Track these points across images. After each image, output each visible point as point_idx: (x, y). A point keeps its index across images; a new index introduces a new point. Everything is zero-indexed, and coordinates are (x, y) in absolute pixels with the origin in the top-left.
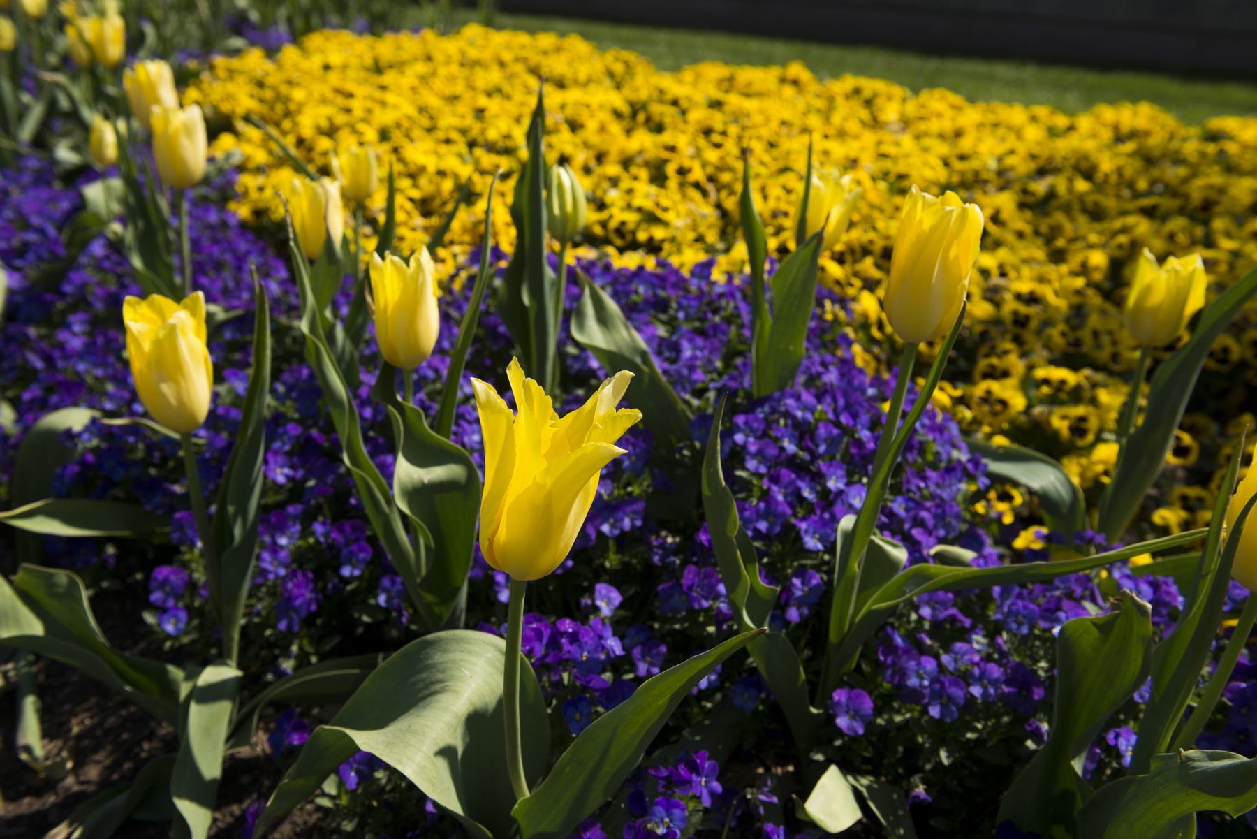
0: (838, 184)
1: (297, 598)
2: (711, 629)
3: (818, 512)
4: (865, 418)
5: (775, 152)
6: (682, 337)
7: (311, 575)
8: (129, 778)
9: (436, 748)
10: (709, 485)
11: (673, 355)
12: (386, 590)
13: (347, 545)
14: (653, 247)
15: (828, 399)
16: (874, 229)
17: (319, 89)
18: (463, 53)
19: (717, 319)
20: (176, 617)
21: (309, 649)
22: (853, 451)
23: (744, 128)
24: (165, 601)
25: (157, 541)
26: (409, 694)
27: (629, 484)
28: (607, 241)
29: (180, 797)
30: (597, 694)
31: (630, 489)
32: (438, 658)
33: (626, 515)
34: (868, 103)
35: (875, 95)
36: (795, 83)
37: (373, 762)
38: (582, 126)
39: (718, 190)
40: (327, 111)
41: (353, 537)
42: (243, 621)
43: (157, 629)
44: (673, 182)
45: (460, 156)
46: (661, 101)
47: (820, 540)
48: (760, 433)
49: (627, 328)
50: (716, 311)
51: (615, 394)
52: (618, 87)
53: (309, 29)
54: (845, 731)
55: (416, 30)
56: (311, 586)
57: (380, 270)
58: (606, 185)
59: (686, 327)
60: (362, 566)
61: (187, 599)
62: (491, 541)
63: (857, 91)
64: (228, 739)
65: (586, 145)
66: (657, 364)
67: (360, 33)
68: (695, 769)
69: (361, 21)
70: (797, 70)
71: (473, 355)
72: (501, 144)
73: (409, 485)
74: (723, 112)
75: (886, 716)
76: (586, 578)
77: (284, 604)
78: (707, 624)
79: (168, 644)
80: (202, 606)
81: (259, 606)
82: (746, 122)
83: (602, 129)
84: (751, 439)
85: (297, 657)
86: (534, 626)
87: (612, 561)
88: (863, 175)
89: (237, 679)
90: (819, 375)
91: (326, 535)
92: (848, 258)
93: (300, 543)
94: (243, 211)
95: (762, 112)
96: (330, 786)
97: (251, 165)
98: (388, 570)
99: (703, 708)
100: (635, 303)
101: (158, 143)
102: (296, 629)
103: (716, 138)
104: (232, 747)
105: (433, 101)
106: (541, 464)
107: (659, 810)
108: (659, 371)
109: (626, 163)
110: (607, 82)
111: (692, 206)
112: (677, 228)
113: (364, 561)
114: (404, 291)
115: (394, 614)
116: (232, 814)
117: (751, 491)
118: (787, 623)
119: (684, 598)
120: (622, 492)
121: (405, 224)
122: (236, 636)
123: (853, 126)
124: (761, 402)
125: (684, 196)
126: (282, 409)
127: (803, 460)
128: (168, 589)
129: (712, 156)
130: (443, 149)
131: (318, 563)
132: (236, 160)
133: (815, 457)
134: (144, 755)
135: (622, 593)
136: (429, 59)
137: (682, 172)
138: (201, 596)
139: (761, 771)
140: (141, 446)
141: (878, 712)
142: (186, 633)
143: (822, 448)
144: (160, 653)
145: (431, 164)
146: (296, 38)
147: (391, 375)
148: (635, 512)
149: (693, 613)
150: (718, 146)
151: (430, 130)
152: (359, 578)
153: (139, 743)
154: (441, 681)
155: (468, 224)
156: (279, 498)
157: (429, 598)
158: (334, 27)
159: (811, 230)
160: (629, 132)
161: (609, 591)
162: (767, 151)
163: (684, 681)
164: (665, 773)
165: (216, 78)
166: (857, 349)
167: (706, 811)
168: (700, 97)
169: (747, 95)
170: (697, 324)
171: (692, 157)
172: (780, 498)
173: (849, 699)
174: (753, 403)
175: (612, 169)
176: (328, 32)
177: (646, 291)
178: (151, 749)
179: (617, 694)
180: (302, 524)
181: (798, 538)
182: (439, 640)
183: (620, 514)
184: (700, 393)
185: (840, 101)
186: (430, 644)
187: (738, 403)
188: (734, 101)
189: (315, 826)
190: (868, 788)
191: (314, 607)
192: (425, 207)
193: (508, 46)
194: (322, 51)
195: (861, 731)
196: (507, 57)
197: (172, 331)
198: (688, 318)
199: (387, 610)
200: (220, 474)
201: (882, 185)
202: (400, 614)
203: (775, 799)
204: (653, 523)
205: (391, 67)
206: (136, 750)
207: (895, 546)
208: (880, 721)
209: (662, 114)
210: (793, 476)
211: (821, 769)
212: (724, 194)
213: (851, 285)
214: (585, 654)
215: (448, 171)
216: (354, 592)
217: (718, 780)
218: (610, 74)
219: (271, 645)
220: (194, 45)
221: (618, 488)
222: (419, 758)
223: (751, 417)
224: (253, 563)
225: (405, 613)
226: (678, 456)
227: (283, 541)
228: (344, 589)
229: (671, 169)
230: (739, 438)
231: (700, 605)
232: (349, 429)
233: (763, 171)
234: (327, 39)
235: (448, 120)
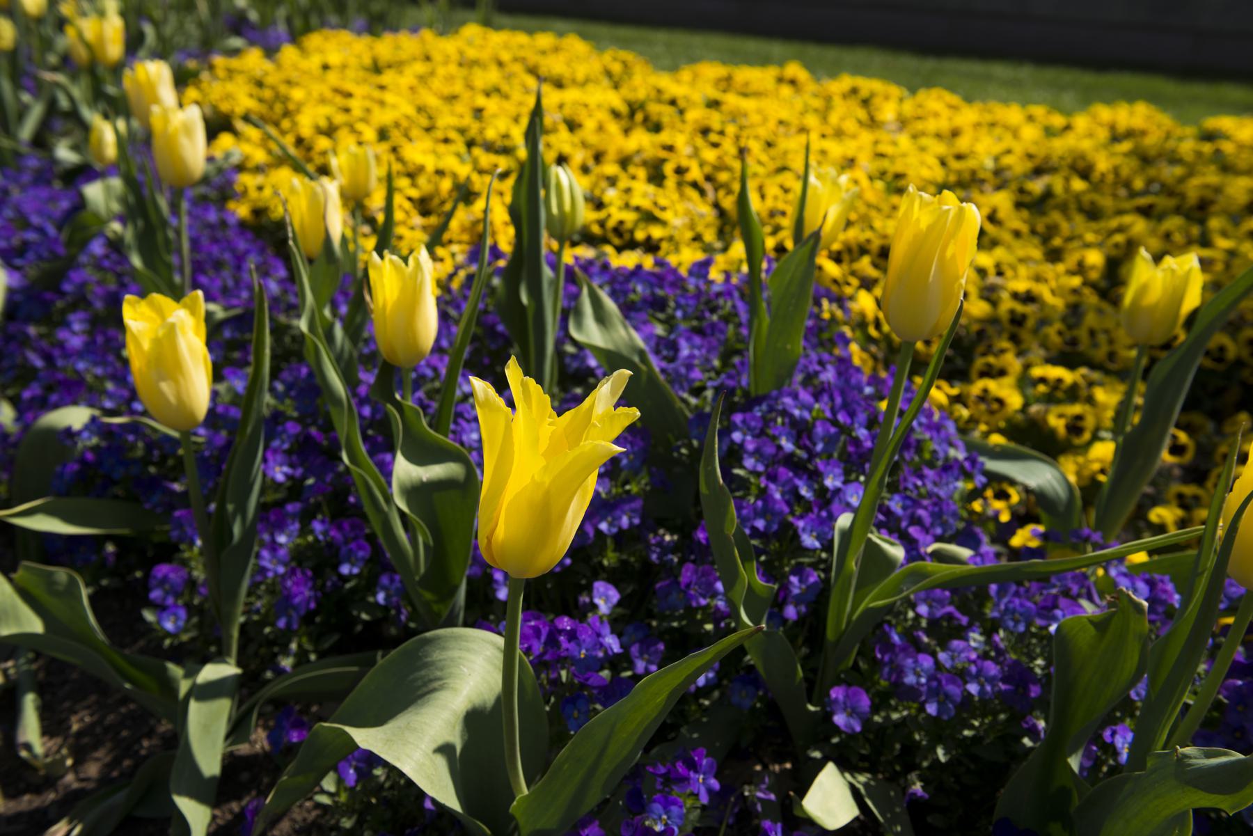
0: (835, 183)
1: (296, 595)
2: (709, 627)
3: (816, 510)
4: (862, 416)
5: (773, 152)
6: (680, 335)
7: (310, 573)
9: (435, 746)
10: (707, 484)
11: (671, 353)
12: (384, 588)
13: (346, 543)
14: (651, 246)
15: (826, 398)
16: (872, 228)
17: (318, 89)
18: (461, 53)
19: (715, 318)
20: (175, 614)
21: (308, 646)
22: (850, 449)
23: (741, 128)
24: (164, 599)
25: (156, 539)
26: (408, 692)
27: (627, 482)
28: (605, 240)
29: (180, 794)
30: (595, 692)
31: (628, 487)
32: (436, 655)
33: (624, 513)
34: (866, 103)
35: (872, 95)
36: (793, 82)
37: (371, 759)
38: (580, 126)
39: (716, 190)
40: (326, 110)
41: (352, 535)
42: (242, 619)
43: (157, 627)
44: (671, 182)
45: (458, 155)
46: (659, 101)
47: (818, 538)
48: (757, 431)
49: (625, 327)
50: (713, 310)
51: (613, 392)
52: (616, 86)
53: (308, 29)
54: (843, 728)
55: (414, 30)
56: (310, 584)
57: (379, 269)
58: (604, 184)
59: (684, 326)
60: (361, 564)
61: (186, 597)
62: (489, 539)
63: (854, 91)
64: (227, 737)
65: (584, 145)
66: (655, 363)
67: (359, 33)
68: (693, 766)
69: (360, 21)
70: (794, 69)
71: (472, 354)
72: (499, 143)
73: (408, 484)
74: (721, 112)
75: (883, 714)
76: (584, 576)
77: (283, 602)
78: (704, 621)
79: (167, 642)
80: (201, 604)
81: (259, 604)
82: (743, 121)
83: (601, 128)
84: (749, 438)
85: (296, 655)
86: (533, 623)
87: (610, 559)
89: (236, 676)
90: (817, 374)
91: (325, 533)
92: (846, 257)
93: (299, 541)
94: (242, 211)
95: (759, 111)
96: (329, 783)
97: (250, 165)
98: (387, 568)
99: (701, 705)
100: (633, 302)
101: (158, 143)
102: (295, 626)
103: (713, 137)
104: (231, 744)
105: (432, 101)
106: (539, 462)
107: (657, 807)
108: (657, 370)
109: (624, 162)
110: (605, 82)
111: (690, 206)
112: (675, 228)
113: (363, 559)
114: (403, 290)
115: (393, 612)
116: (231, 811)
117: (748, 489)
118: (784, 621)
119: (681, 595)
120: (620, 490)
121: (404, 223)
122: (235, 633)
123: (850, 126)
124: (758, 400)
125: (682, 195)
126: (281, 408)
127: (800, 458)
128: (167, 587)
129: (710, 155)
130: (442, 148)
131: (317, 561)
132: (235, 159)
133: (812, 455)
134: (143, 752)
135: (620, 591)
136: (428, 58)
137: (680, 171)
138: (200, 594)
139: (758, 768)
140: (140, 444)
141: (875, 709)
142: (186, 630)
143: (819, 447)
144: (159, 650)
145: (430, 163)
146: (295, 37)
147: (390, 374)
148: (633, 511)
149: (690, 611)
150: (715, 145)
151: (428, 130)
152: (358, 576)
153: (138, 741)
154: (440, 679)
155: (467, 224)
156: (278, 496)
157: (428, 596)
158: (333, 27)
159: (809, 229)
160: (627, 132)
161: (607, 589)
162: (764, 150)
163: (682, 679)
164: (663, 770)
166: (854, 347)
167: (704, 808)
168: (697, 97)
169: (745, 95)
170: (695, 323)
171: (690, 157)
172: (778, 496)
173: (847, 696)
175: (610, 169)
176: (327, 32)
177: (644, 290)
178: (150, 747)
179: (615, 691)
180: (301, 522)
181: (796, 537)
182: (438, 638)
183: (618, 512)
184: (698, 392)
185: (837, 101)
186: (428, 642)
187: (736, 402)
188: (732, 100)
189: (314, 823)
190: (866, 785)
191: (313, 605)
192: (424, 206)
193: (506, 46)
194: (321, 51)
195: (858, 728)
196: (506, 56)
197: (171, 330)
198: (686, 317)
199: (386, 608)
200: (219, 472)
201: (880, 185)
202: (399, 612)
203: (772, 797)
204: (651, 521)
205: (389, 66)
206: (136, 747)
207: (892, 544)
208: (877, 718)
209: (660, 114)
210: (791, 474)
211: (819, 766)
212: (721, 193)
213: (848, 284)
214: (583, 651)
215: (447, 171)
216: (352, 590)
217: (716, 777)
218: (608, 74)
219: (270, 642)
220: (194, 45)
221: (616, 486)
222: (418, 755)
223: (748, 415)
224: (252, 561)
225: (404, 611)
226: (675, 454)
227: (282, 539)
228: (343, 587)
229: (668, 169)
230: (737, 436)
231: (698, 603)
232: (348, 428)
234: (326, 39)
235: (447, 120)
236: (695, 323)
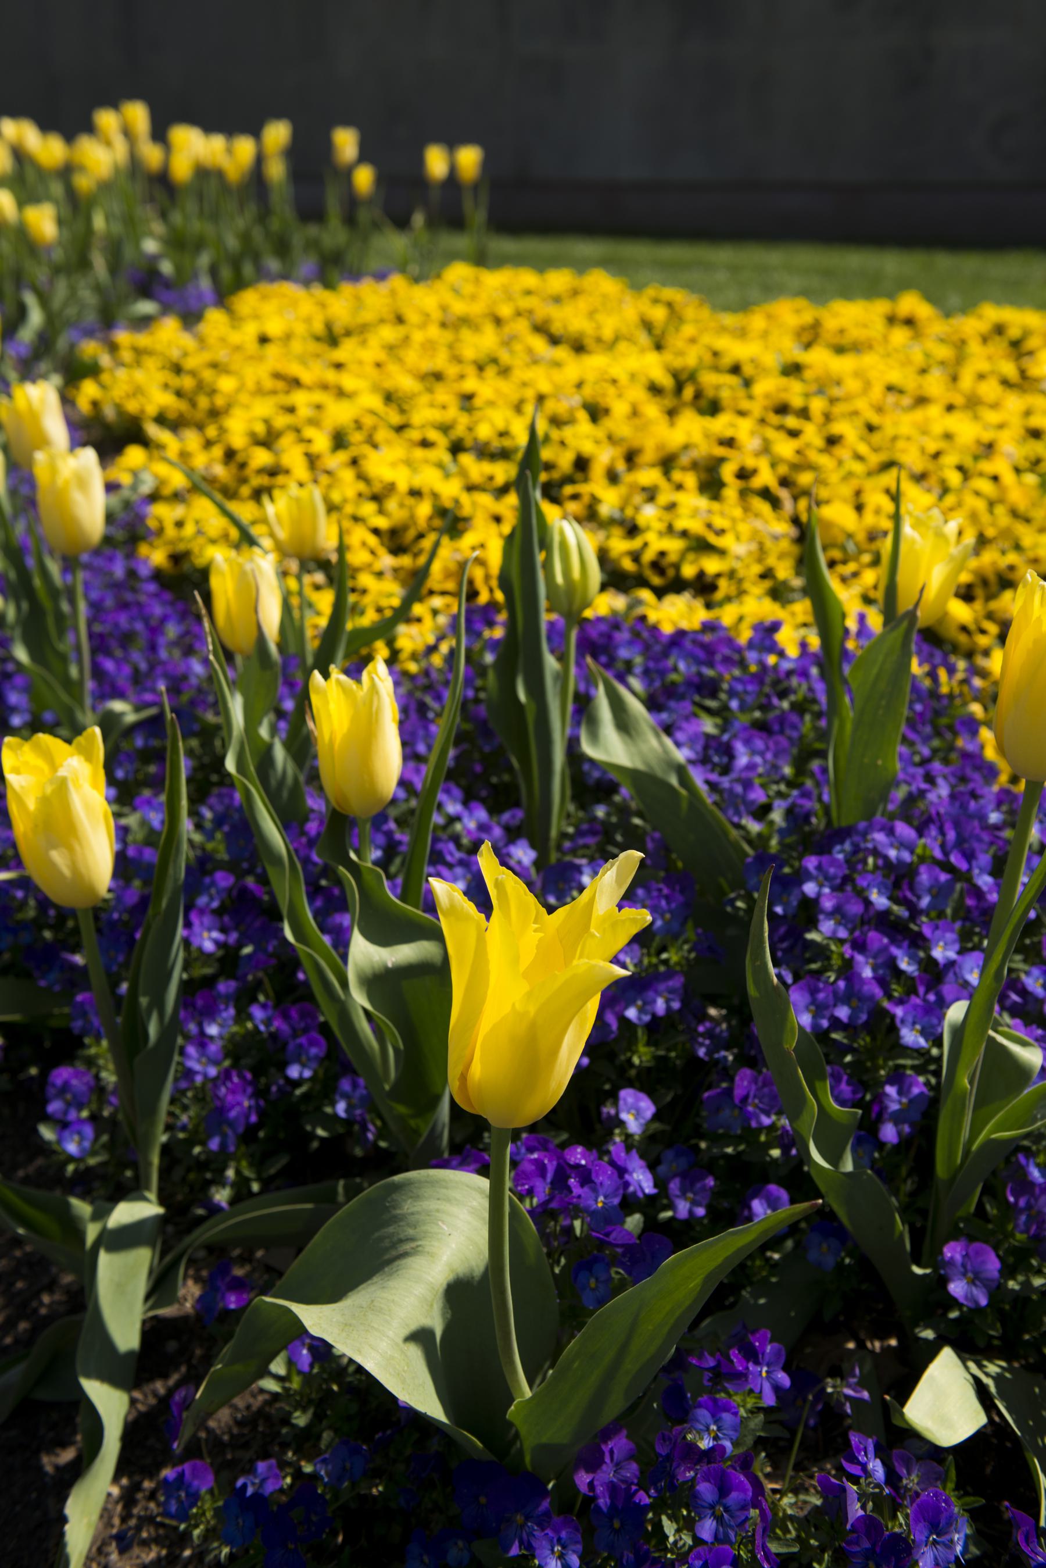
0: (939, 535)
1: (232, 1107)
2: (776, 1153)
3: (921, 990)
4: (984, 858)
5: (876, 438)
6: (735, 736)
7: (249, 1076)
8: (26, 1342)
9: (406, 1332)
10: (756, 983)
11: (725, 760)
12: (346, 1096)
13: (295, 1036)
14: (704, 587)
15: (933, 832)
16: (1018, 547)
17: (257, 373)
18: (444, 308)
19: (785, 705)
20: (79, 1133)
21: (247, 1173)
22: (970, 902)
23: (833, 401)
24: (66, 1113)
25: (54, 1023)
26: (373, 1254)
27: (664, 949)
28: (642, 582)
29: (89, 1376)
30: (619, 1250)
31: (664, 956)
32: (408, 1207)
33: (660, 995)
34: (1018, 348)
35: (1027, 333)
36: (909, 322)
37: (322, 1350)
38: (607, 411)
39: (795, 498)
40: (264, 408)
41: (302, 1025)
42: (164, 1138)
43: (55, 1147)
44: (731, 493)
45: (440, 466)
46: (716, 369)
47: (923, 1033)
49: (658, 736)
50: (783, 695)
51: (619, 881)
52: (659, 347)
53: (240, 284)
54: (962, 1300)
55: (381, 276)
56: (250, 1090)
57: (323, 693)
58: (638, 499)
59: (744, 719)
60: (314, 1065)
61: (94, 1106)
62: (463, 1078)
63: (999, 329)
64: (147, 1298)
65: (611, 438)
66: (698, 777)
67: (306, 283)
68: (752, 1355)
69: (307, 264)
70: (911, 303)
71: (457, 759)
72: (496, 444)
73: (369, 971)
74: (803, 380)
75: (1021, 1278)
76: (608, 1080)
77: (216, 1117)
78: (769, 1145)
79: (71, 1168)
80: (113, 1115)
81: (184, 1118)
82: (835, 392)
83: (635, 413)
84: (826, 890)
85: (233, 1185)
86: (535, 1156)
87: (641, 1056)
88: (1000, 466)
89: (157, 1218)
90: (922, 793)
91: (268, 1022)
92: (979, 592)
93: (235, 1029)
94: (157, 557)
95: (858, 374)
96: (278, 1366)
97: (167, 491)
98: (347, 1068)
99: (768, 1260)
100: (673, 684)
101: (43, 498)
102: (232, 1149)
103: (791, 422)
104: (151, 1308)
105: (406, 383)
106: (528, 973)
107: (703, 1414)
108: (702, 788)
109: (667, 463)
110: (643, 339)
111: (758, 524)
112: (738, 558)
113: (316, 1057)
114: (355, 720)
115: (356, 1127)
116: (155, 1394)
117: (829, 958)
118: (880, 1145)
119: (736, 1112)
120: (654, 960)
121: (368, 567)
122: (155, 1160)
123: (990, 390)
124: (839, 835)
125: (747, 509)
126: (210, 846)
127: (898, 917)
128: (69, 1097)
129: (785, 448)
130: (419, 453)
131: (258, 1058)
133: (915, 912)
134: (43, 1311)
135: (655, 1101)
136: (400, 320)
137: (744, 474)
138: (111, 1104)
139: (851, 1345)
140: (32, 902)
141: (1009, 1271)
142: (94, 1153)
143: (925, 901)
144: (57, 1179)
145: (403, 479)
146: (222, 297)
147: (340, 825)
148: (671, 991)
149: (749, 1135)
150: (794, 434)
151: (400, 429)
152: (311, 1079)
153: (37, 1295)
154: (412, 1239)
155: (453, 566)
156: (208, 971)
157: (402, 1109)
158: (272, 278)
159: (904, 604)
160: (672, 413)
161: (638, 1100)
162: (862, 439)
163: (720, 1260)
164: (711, 1363)
165: (120, 364)
166: (986, 735)
167: (767, 1411)
168: (771, 361)
169: (840, 350)
170: (757, 714)
171: (757, 454)
172: (867, 973)
173: (966, 1256)
174: (823, 844)
175: (649, 476)
176: (265, 287)
177: (688, 667)
178: (52, 1303)
179: (642, 1257)
180: (236, 1007)
181: (893, 1029)
182: (409, 1183)
183: (651, 994)
184: (762, 812)
185: (974, 347)
186: (398, 1187)
187: (809, 836)
188: (819, 359)
189: (260, 1412)
190: (998, 1379)
191: (254, 1118)
192: (396, 540)
193: (508, 295)
194: (256, 317)
195: (983, 1302)
196: (505, 311)
197: (62, 787)
198: (743, 708)
199: (348, 1122)
200: (131, 942)
201: (1031, 479)
202: (364, 1129)
203: (866, 1395)
204: (692, 1009)
205: (348, 333)
206: (34, 1304)
207: (1024, 1044)
208: (1012, 1284)
209: (718, 387)
210: (885, 940)
211: (930, 1352)
212: (803, 504)
213: (983, 632)
214: (601, 1198)
215: (425, 490)
216: (306, 1096)
217: (786, 1369)
218: (647, 325)
219: (201, 1165)
220: (91, 317)
221: (649, 955)
222: (384, 1345)
223: (825, 859)
224: (176, 1058)
225: (371, 1127)
226: (729, 909)
227: (213, 1030)
228: (292, 1093)
229: (728, 472)
230: (810, 888)
231: (759, 1122)
232: (289, 890)
233: (858, 468)
234: (264, 298)
236: (757, 714)
